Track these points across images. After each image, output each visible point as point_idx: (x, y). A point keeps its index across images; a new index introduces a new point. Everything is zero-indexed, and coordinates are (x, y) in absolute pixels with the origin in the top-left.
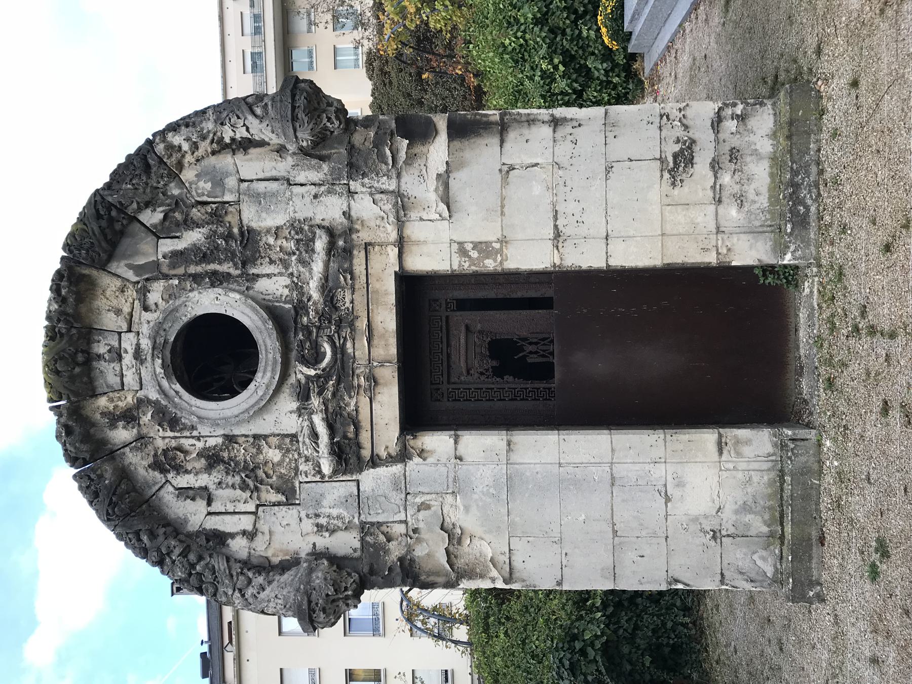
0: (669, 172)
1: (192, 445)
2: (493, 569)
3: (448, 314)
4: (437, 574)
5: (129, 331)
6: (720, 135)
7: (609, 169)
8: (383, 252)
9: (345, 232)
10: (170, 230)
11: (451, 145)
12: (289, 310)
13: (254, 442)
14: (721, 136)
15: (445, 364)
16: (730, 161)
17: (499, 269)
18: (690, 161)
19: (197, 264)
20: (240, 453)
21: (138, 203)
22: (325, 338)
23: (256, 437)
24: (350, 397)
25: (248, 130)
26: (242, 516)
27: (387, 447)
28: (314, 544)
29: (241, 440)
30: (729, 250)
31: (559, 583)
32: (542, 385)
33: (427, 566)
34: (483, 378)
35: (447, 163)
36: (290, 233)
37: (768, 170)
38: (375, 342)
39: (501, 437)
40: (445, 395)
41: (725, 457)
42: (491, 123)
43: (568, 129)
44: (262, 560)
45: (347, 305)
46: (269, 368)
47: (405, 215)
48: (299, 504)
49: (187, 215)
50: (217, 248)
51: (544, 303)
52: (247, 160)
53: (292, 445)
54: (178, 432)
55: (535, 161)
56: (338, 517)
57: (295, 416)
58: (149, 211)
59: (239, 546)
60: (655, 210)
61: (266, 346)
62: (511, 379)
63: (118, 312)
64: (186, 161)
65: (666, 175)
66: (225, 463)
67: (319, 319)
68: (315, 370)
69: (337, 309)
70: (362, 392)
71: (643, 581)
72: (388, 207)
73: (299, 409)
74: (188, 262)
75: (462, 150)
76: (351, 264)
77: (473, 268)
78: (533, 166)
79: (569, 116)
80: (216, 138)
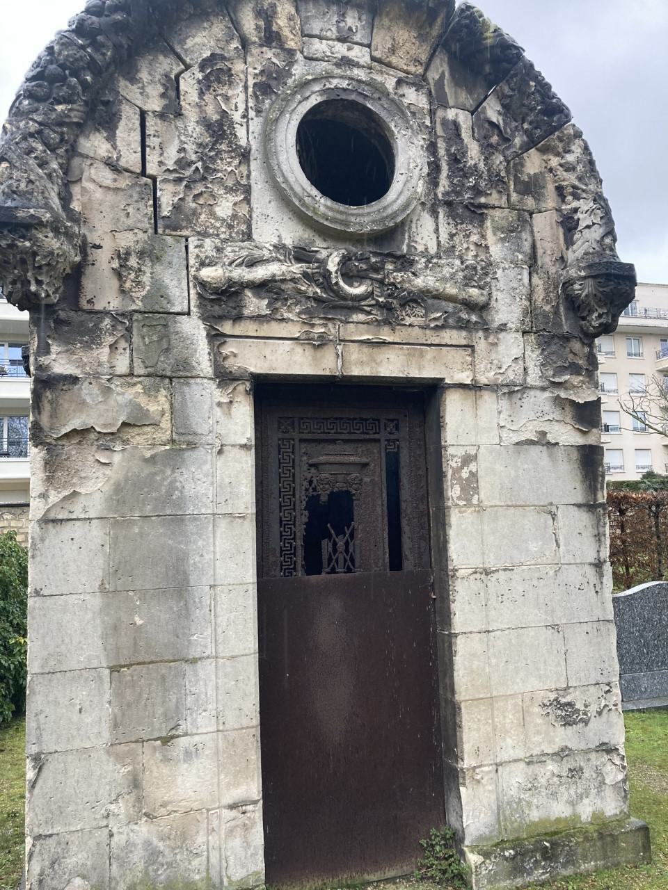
0: (556, 699)
1: (236, 107)
2: (61, 496)
3: (382, 441)
4: (54, 415)
5: (373, 59)
6: (594, 753)
7: (555, 627)
8: (465, 366)
9: (487, 324)
10: (480, 127)
11: (573, 448)
12: (399, 248)
13: (240, 185)
14: (593, 756)
15: (363, 437)
16: (570, 769)
17: (449, 503)
18: (567, 723)
19: (447, 150)
20: (227, 165)
21: (510, 96)
22: (370, 289)
23: (248, 190)
24: (300, 313)
25: (588, 227)
26: (139, 155)
27: (235, 355)
28: (99, 247)
29: (243, 169)
30: (478, 782)
31: (37, 593)
32: (300, 561)
33: (65, 403)
34: (305, 483)
35: (557, 444)
36: (482, 261)
37: (563, 816)
38: (365, 349)
39: (249, 506)
40: (287, 436)
41: (228, 814)
42: (595, 495)
43: (593, 579)
44: (77, 173)
45: (407, 318)
46: (339, 216)
47: (504, 394)
48: (156, 232)
49: (496, 149)
50: (465, 176)
51: (396, 561)
52: (551, 224)
53: (237, 233)
54: (255, 93)
55: (561, 543)
56: (139, 283)
57: (275, 241)
58: (499, 108)
59: (95, 144)
60: (518, 687)
61: (362, 215)
62: (305, 520)
63: (393, 51)
64: (551, 157)
65: (552, 696)
66: (214, 144)
67: (393, 284)
68: (336, 272)
69: (403, 306)
70: (306, 328)
71: (42, 717)
72: (511, 376)
73: (284, 247)
74: (449, 141)
75: (570, 460)
76: (451, 328)
77: (449, 473)
78: (556, 541)
79: (604, 580)
80: (579, 191)
